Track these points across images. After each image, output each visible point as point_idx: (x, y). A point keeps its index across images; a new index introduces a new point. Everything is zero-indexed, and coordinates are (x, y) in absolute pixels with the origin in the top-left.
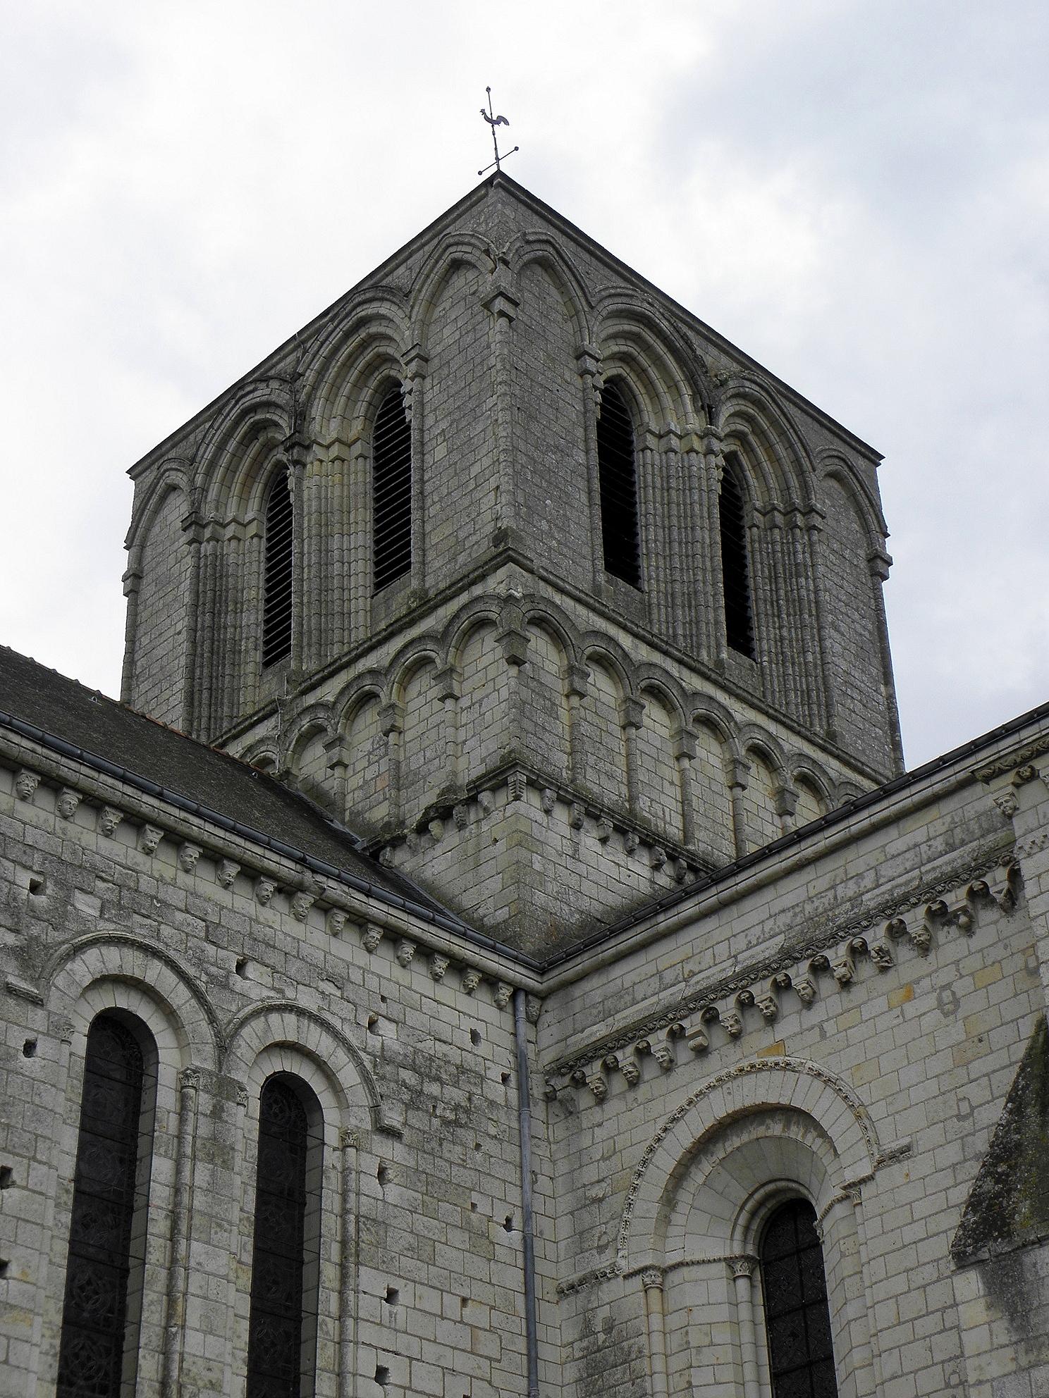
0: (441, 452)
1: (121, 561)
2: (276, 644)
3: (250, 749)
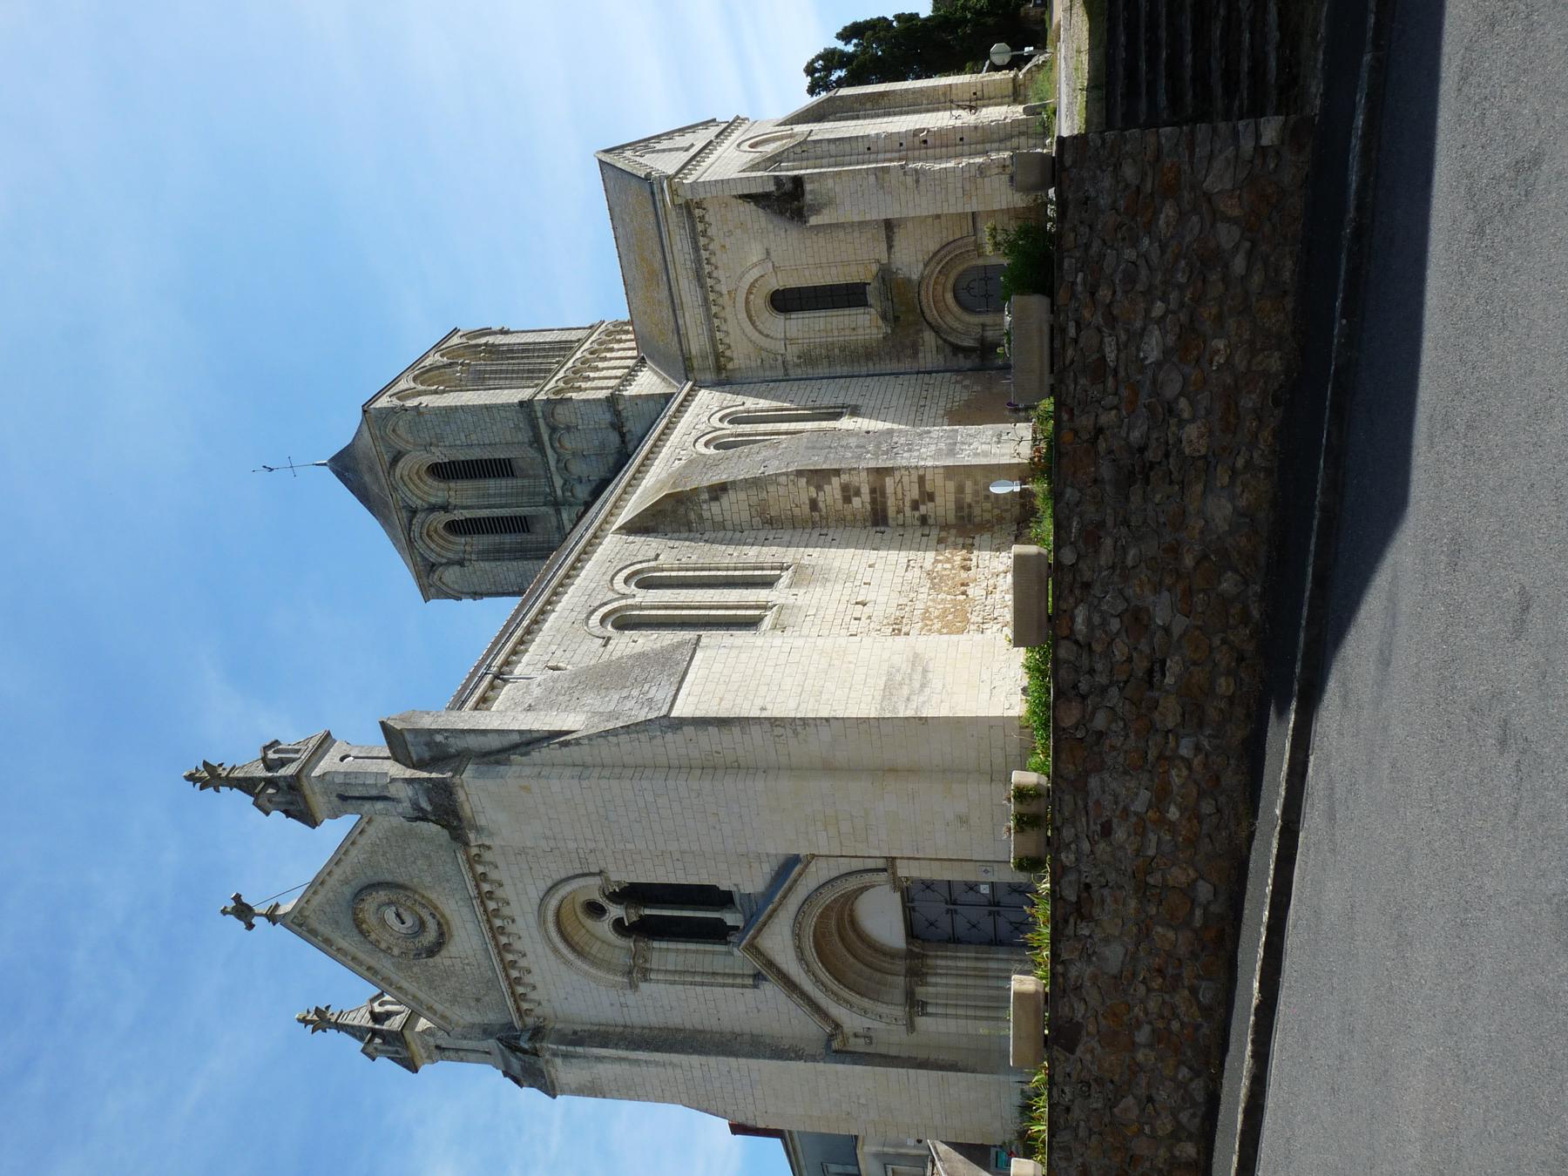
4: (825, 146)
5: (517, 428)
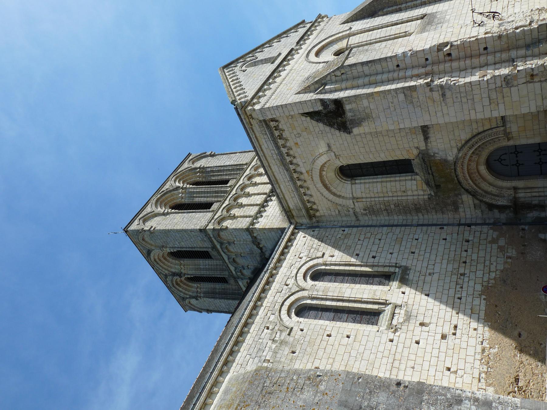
0: (183, 243)
1: (204, 314)
2: (223, 280)
3: (244, 286)
4: (360, 68)
5: (203, 240)
